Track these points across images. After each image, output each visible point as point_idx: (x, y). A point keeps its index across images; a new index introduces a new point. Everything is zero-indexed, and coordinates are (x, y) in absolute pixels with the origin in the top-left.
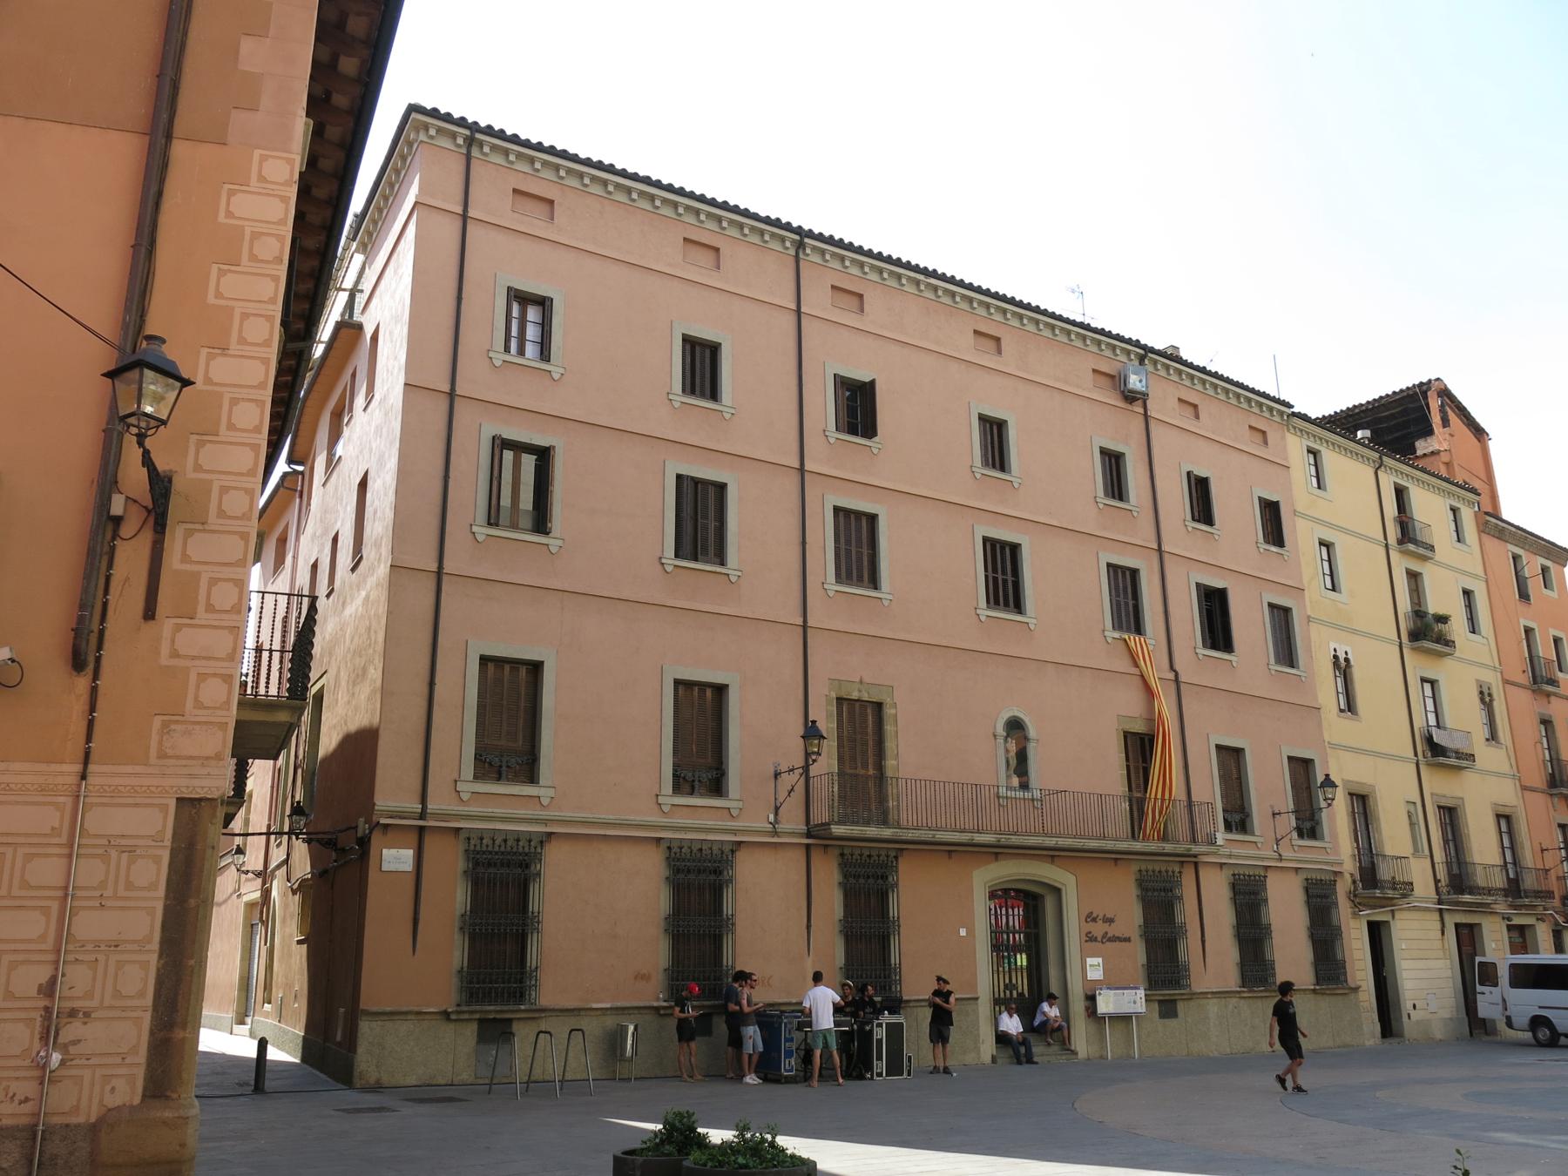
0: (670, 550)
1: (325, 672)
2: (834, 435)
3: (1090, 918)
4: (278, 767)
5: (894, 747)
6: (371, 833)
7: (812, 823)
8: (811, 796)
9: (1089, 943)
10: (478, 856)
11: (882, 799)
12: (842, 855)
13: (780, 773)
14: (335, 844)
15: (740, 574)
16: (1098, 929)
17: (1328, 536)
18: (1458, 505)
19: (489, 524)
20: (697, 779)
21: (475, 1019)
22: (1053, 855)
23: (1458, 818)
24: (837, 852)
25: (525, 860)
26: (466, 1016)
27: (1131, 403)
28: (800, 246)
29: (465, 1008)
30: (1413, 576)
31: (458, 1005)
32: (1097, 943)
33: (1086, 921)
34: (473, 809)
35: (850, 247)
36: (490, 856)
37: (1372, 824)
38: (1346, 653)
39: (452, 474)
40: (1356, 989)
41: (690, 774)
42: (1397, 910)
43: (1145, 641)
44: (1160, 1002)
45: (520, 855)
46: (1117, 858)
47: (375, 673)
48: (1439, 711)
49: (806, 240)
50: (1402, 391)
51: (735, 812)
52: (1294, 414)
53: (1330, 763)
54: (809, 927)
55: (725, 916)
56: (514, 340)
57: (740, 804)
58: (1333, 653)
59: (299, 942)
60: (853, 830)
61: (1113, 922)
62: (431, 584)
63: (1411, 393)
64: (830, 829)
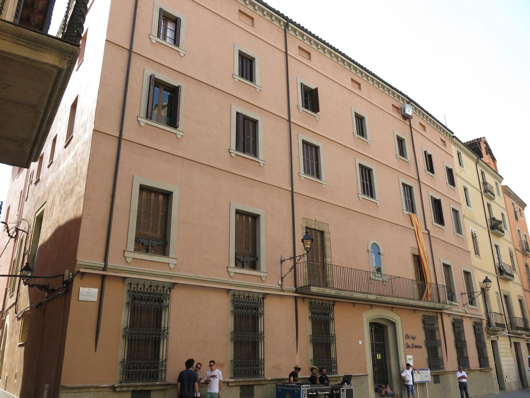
0: (233, 147)
1: (45, 202)
2: (302, 109)
3: (407, 337)
4: (13, 259)
5: (330, 252)
6: (73, 277)
7: (298, 286)
8: (297, 274)
9: (407, 348)
10: (136, 294)
11: (325, 277)
12: (311, 303)
13: (284, 260)
14: (47, 289)
15: (264, 163)
16: (410, 342)
17: (467, 186)
18: (497, 182)
19: (147, 117)
20: (245, 261)
21: (130, 391)
22: (393, 306)
23: (509, 300)
24: (307, 301)
25: (161, 298)
26: (125, 389)
27: (405, 120)
28: (287, 26)
29: (125, 384)
30: (489, 205)
31: (120, 382)
32: (410, 349)
33: (406, 338)
34: (133, 267)
35: (306, 31)
36: (142, 295)
37: (487, 300)
38: (475, 231)
39: (129, 89)
40: (491, 369)
41: (242, 258)
42: (499, 336)
43: (417, 217)
44: (241, 386)
45: (158, 295)
46: (415, 309)
47: (81, 189)
48: (499, 258)
49: (290, 24)
50: (470, 141)
51: (263, 279)
52: (454, 137)
53: (475, 274)
54: (297, 339)
55: (260, 333)
56: (161, 34)
57: (266, 275)
58: (471, 231)
59: (20, 346)
60: (320, 289)
61: (415, 339)
62: (115, 143)
63: (473, 142)
64: (310, 288)
